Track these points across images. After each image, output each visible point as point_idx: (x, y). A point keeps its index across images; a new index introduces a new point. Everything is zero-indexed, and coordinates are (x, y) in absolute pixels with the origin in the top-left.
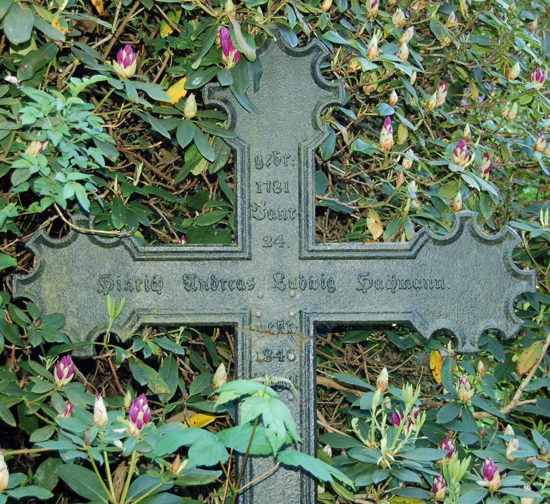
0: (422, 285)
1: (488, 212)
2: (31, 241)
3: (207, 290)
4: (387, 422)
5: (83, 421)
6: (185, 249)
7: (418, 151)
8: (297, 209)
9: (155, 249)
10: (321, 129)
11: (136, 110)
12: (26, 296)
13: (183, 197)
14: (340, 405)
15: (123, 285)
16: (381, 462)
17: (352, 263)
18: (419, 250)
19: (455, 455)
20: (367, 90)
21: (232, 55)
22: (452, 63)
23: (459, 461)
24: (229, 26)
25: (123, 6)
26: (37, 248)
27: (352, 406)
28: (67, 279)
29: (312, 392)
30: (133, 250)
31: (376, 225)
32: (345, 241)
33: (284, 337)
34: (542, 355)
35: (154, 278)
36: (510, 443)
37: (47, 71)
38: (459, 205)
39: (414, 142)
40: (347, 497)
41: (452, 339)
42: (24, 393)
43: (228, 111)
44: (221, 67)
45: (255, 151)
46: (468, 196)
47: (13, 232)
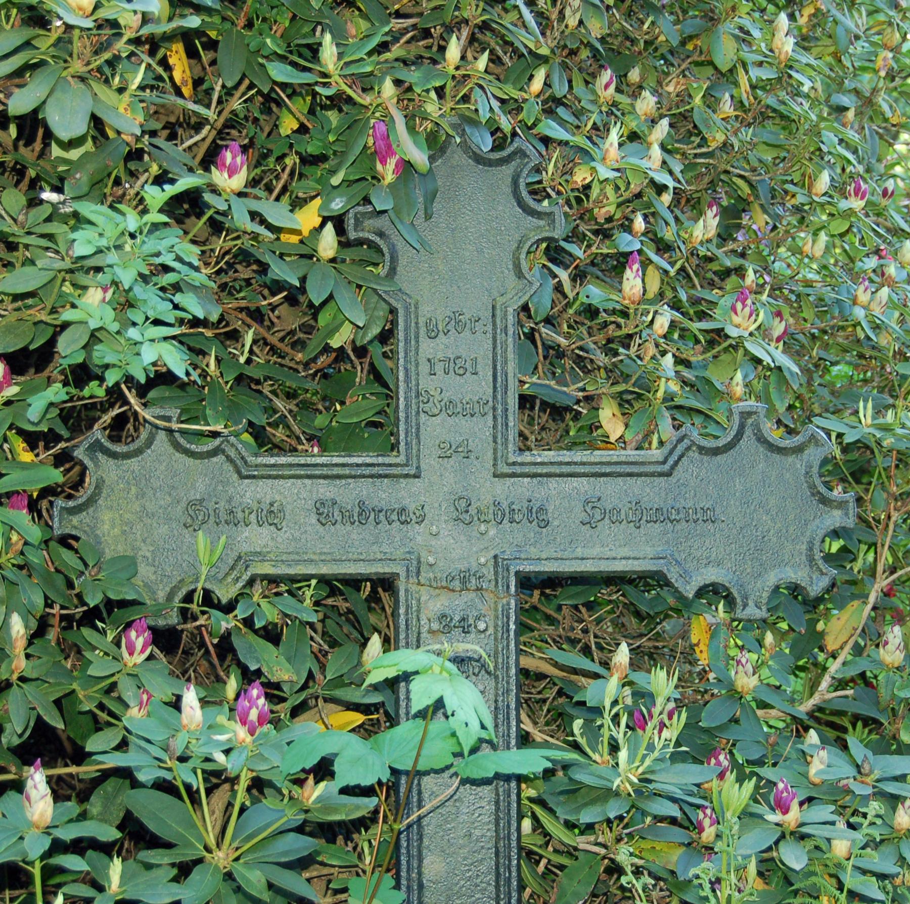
0: (682, 516)
1: (782, 400)
2: (82, 449)
3: (353, 523)
4: (628, 726)
5: (165, 724)
6: (319, 460)
7: (676, 305)
8: (491, 399)
9: (272, 461)
10: (527, 276)
11: (246, 243)
12: (74, 533)
13: (313, 379)
14: (554, 699)
15: (223, 517)
16: (618, 786)
17: (575, 482)
18: (676, 463)
19: (731, 777)
20: (601, 213)
21: (392, 163)
22: (727, 172)
23: (737, 785)
24: (387, 118)
25: (223, 86)
26: (92, 459)
27: (575, 700)
28: (136, 507)
29: (513, 680)
30: (239, 462)
31: (614, 419)
32: (561, 448)
33: (469, 596)
34: (863, 622)
35: (272, 505)
36: (815, 758)
37: (110, 184)
38: (739, 390)
39: (669, 294)
40: (566, 840)
41: (725, 597)
42: (75, 679)
43: (385, 250)
44: (374, 182)
45: (425, 311)
46: (751, 377)
47: (57, 431)
